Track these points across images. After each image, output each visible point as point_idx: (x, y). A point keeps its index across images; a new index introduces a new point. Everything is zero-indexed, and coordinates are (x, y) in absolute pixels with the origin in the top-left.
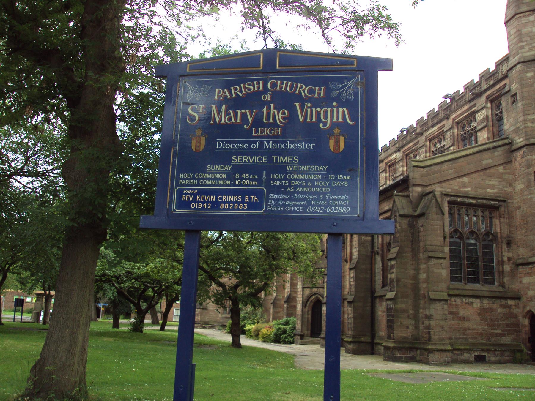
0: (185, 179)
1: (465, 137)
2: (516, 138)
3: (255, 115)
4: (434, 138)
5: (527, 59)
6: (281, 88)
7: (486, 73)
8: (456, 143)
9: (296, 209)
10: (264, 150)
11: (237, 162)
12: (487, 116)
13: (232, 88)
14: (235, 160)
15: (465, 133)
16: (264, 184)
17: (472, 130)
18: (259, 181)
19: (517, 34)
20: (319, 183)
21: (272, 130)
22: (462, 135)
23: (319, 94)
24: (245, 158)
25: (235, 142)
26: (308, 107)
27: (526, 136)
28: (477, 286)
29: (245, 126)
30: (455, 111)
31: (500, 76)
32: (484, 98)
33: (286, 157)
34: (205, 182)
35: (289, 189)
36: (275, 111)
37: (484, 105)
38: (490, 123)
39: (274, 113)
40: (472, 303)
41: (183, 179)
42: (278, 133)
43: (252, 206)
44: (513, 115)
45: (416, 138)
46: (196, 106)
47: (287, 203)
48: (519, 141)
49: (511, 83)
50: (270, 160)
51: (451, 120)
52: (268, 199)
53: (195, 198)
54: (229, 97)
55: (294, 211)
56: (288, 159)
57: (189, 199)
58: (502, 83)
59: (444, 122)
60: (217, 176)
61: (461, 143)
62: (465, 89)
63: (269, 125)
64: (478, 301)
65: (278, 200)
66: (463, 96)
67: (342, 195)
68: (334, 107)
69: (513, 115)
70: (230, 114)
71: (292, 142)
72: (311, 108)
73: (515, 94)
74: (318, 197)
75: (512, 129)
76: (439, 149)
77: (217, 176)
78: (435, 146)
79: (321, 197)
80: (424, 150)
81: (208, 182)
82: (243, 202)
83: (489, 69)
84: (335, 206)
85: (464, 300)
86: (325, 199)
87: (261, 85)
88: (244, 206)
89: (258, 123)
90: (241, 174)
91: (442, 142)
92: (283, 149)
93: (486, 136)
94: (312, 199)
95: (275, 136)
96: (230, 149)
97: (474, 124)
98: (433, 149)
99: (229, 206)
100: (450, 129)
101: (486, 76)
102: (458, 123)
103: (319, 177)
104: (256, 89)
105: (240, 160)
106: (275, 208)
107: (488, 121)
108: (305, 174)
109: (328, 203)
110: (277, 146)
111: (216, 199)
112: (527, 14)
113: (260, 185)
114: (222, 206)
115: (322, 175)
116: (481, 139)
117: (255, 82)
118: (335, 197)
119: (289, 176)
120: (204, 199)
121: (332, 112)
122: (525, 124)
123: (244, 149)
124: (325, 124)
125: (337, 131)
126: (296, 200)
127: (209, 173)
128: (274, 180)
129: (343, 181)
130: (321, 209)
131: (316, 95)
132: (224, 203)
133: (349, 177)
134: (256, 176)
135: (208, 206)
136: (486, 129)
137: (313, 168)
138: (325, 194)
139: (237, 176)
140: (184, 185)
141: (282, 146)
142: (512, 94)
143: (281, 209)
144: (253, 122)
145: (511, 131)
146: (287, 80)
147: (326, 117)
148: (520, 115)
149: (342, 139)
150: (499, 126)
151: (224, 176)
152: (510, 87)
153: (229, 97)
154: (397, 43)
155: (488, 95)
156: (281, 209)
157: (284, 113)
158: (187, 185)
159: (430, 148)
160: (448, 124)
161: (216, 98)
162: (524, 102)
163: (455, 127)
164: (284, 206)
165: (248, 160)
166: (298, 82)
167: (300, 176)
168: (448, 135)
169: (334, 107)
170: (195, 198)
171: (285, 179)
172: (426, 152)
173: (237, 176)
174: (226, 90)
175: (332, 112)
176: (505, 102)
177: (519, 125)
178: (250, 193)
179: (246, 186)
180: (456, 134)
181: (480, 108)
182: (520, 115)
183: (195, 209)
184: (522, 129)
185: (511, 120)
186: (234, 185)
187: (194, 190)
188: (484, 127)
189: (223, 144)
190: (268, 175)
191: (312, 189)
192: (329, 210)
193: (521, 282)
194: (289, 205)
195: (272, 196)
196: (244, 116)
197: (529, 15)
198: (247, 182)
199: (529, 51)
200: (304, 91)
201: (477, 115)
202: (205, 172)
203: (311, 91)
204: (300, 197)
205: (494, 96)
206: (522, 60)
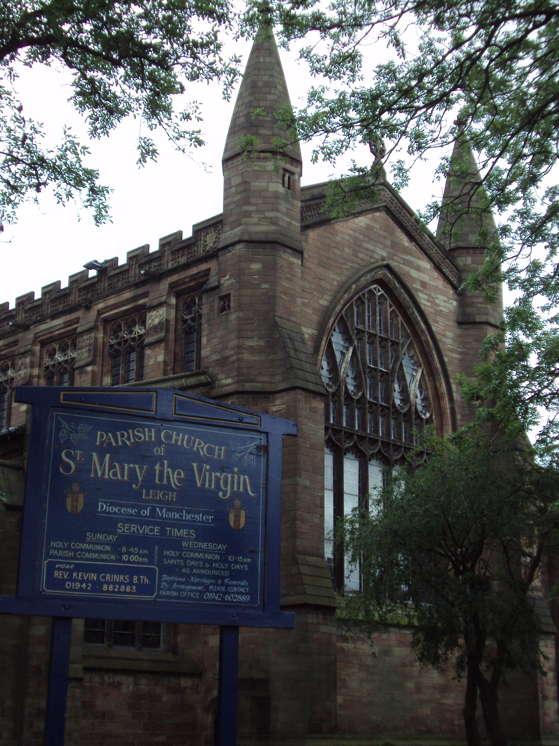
0: (58, 549)
1: (117, 351)
2: (220, 377)
3: (146, 472)
4: (52, 340)
5: (254, 237)
6: (177, 441)
7: (175, 240)
8: (99, 359)
9: (192, 595)
10: (156, 518)
11: (124, 531)
12: (167, 321)
13: (118, 433)
14: (121, 529)
15: (119, 344)
16: (156, 562)
17: (134, 339)
18: (150, 556)
19: (241, 188)
20: (217, 565)
21: (166, 494)
22: (111, 346)
23: (219, 455)
24: (134, 527)
25: (122, 506)
26: (206, 470)
27: (239, 375)
28: (130, 651)
29: (134, 486)
30: (105, 297)
31: (200, 251)
32: (164, 285)
33: (182, 531)
34: (84, 555)
35: (184, 570)
36: (170, 470)
37: (164, 298)
38: (172, 336)
39: (168, 472)
40: (119, 684)
41: (55, 548)
42: (172, 498)
43: (142, 589)
44: (219, 333)
45: (13, 332)
46: (72, 452)
47: (183, 587)
48: (226, 382)
49: (221, 274)
50: (163, 531)
51: (93, 313)
52: (160, 581)
53: (71, 575)
54: (114, 444)
55: (189, 598)
56: (183, 532)
57: (63, 576)
58: (204, 267)
59: (79, 314)
60: (99, 547)
61: (109, 362)
62: (130, 259)
63: (161, 487)
64: (131, 679)
65: (172, 582)
66: (124, 271)
67: (242, 580)
68: (235, 473)
69: (219, 333)
70: (115, 468)
71: (188, 512)
72: (210, 471)
73: (228, 296)
74: (217, 582)
75: (215, 357)
76: (60, 363)
77: (99, 547)
78: (52, 355)
79: (220, 582)
80: (28, 360)
81: (87, 555)
82: (131, 583)
83: (180, 233)
84: (234, 593)
85: (106, 678)
86: (223, 584)
87: (153, 434)
88: (132, 589)
89: (149, 482)
90: (128, 547)
91: (69, 352)
92: (177, 519)
93: (161, 358)
94: (210, 584)
95: (168, 502)
96: (115, 513)
97: (138, 330)
98: (48, 362)
99: (114, 588)
100: (90, 330)
101: (172, 243)
102: (106, 321)
103: (217, 557)
104: (147, 439)
105: (127, 529)
106: (168, 593)
107: (167, 331)
108: (202, 552)
109: (226, 589)
110: (171, 515)
111: (98, 577)
112: (262, 155)
113: (151, 562)
114: (105, 587)
115: (221, 555)
116: (152, 362)
117: (146, 430)
118: (234, 582)
119: (185, 554)
120: (83, 577)
121: (233, 478)
122: (238, 353)
123: (132, 515)
124: (225, 494)
125: (237, 503)
126: (193, 584)
127: (89, 543)
128: (168, 557)
129: (243, 563)
130: (219, 596)
131: (216, 457)
132: (108, 583)
133: (249, 560)
134: (146, 552)
135: (87, 586)
136: (163, 345)
137: (211, 546)
138: (223, 578)
139: (124, 549)
140: (56, 557)
141: (177, 516)
142: (223, 294)
143: (176, 594)
144: (142, 481)
145: (213, 362)
146: (185, 432)
147: (226, 486)
148: (233, 336)
149: (243, 513)
150: (188, 343)
151: (108, 548)
152: (219, 281)
153: (114, 444)
154: (98, 219)
155: (174, 283)
156: (176, 594)
157: (179, 474)
158: (61, 557)
159: (41, 358)
160: (87, 319)
161: (98, 443)
162: (241, 314)
163: (101, 328)
164: (179, 590)
165: (137, 530)
166: (196, 437)
167: (197, 555)
168: (86, 340)
169: (235, 473)
170: (71, 575)
171: (180, 557)
172: (32, 366)
173: (124, 549)
174: (110, 434)
175: (233, 478)
176: (208, 306)
177: (227, 353)
178: (139, 572)
179: (134, 562)
180: (100, 341)
181: (156, 302)
182: (233, 336)
183: (70, 590)
184: (233, 362)
185: (215, 341)
186: (120, 560)
187: (70, 564)
188: (159, 341)
189: (106, 505)
190: (161, 552)
191: (209, 572)
192: (228, 598)
193: (206, 643)
194: (184, 590)
195: (165, 577)
196: (132, 472)
197: (265, 159)
198: (135, 557)
199: (259, 224)
200: (202, 448)
201: (148, 315)
202: (84, 542)
203: (210, 450)
204: (197, 580)
205: (183, 287)
206: (246, 238)
